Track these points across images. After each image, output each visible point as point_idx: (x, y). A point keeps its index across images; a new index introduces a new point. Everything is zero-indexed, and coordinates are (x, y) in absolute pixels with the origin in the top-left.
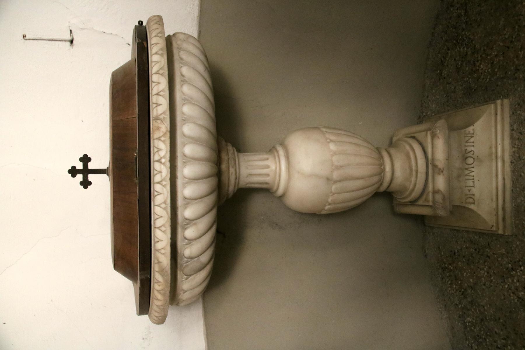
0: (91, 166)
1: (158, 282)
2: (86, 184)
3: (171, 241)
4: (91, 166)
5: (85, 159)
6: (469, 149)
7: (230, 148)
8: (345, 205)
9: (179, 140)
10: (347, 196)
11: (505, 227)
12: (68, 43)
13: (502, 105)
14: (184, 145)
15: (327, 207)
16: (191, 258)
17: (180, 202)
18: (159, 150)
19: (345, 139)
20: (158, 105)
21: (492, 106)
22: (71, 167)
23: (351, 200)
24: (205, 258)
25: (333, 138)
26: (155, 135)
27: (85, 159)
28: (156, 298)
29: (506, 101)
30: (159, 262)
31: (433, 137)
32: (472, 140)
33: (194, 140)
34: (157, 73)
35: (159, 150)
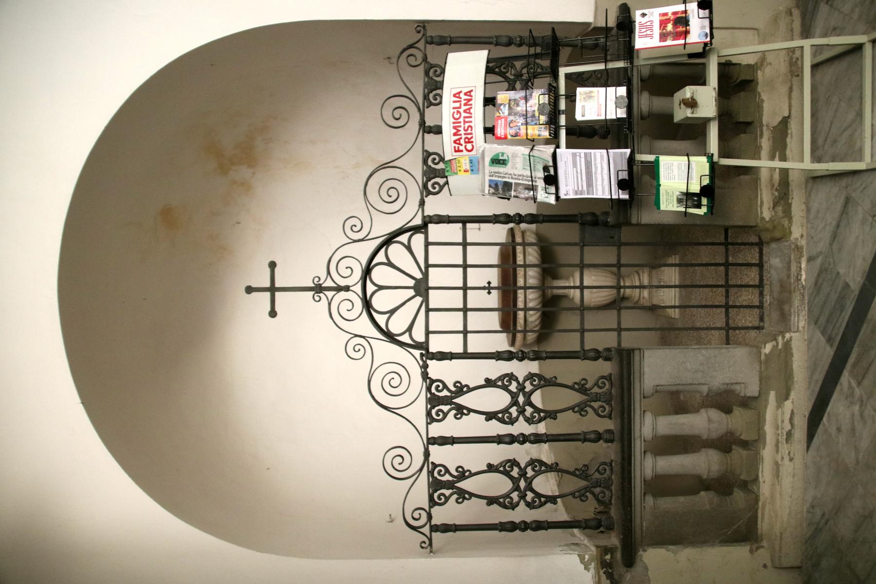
0: (491, 285)
1: (519, 337)
2: (489, 293)
3: (533, 403)
4: (491, 285)
5: (489, 283)
6: (662, 278)
7: (549, 278)
8: (600, 303)
9: (528, 277)
10: (600, 299)
11: (675, 314)
12: (478, 230)
13: (675, 258)
14: (529, 279)
15: (592, 304)
16: (532, 322)
17: (528, 301)
18: (520, 281)
19: (600, 274)
20: (520, 297)
21: (671, 258)
22: (278, 312)
23: (605, 301)
24: (537, 322)
25: (594, 273)
26: (519, 276)
27: (489, 283)
28: (531, 35)
29: (677, 256)
30: (520, 323)
31: (643, 272)
32: (663, 273)
33: (533, 277)
34: (519, 253)
35: (520, 281)
